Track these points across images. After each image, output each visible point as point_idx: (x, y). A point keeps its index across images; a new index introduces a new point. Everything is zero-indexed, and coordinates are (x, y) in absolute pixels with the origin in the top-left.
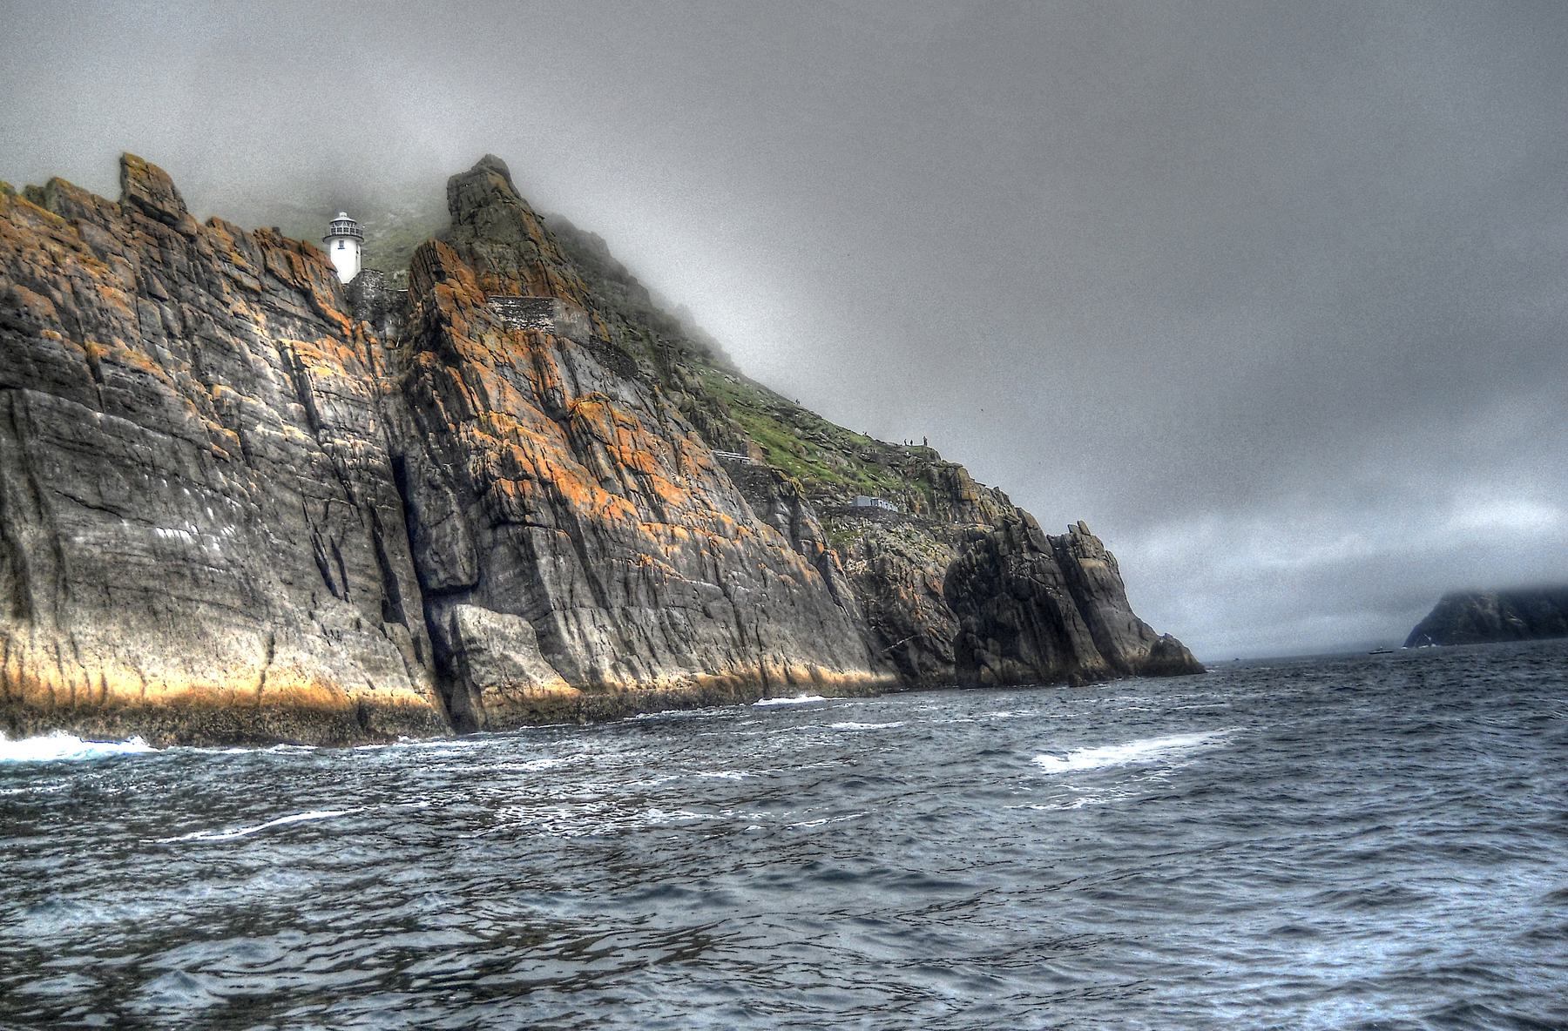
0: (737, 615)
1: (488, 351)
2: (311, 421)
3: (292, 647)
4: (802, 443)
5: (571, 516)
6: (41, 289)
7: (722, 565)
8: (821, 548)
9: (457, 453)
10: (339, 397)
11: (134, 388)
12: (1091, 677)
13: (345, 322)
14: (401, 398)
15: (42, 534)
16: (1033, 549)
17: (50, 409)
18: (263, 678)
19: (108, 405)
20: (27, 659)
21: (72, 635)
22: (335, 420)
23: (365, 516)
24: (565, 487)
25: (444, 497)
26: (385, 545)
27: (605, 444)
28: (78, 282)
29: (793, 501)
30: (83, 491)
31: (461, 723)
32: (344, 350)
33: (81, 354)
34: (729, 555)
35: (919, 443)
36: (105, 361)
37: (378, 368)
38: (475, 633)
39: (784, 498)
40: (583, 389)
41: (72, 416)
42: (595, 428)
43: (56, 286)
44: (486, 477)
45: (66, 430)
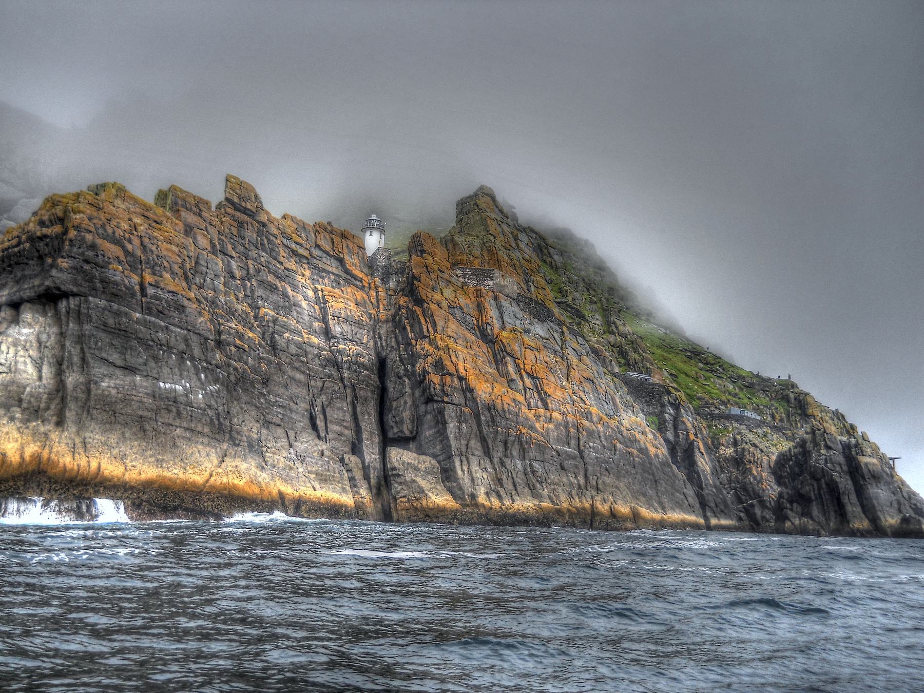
0: (586, 470)
1: (441, 296)
2: (327, 333)
3: (237, 460)
4: (703, 372)
5: (474, 400)
6: (118, 242)
7: (583, 439)
8: (692, 437)
9: (413, 357)
10: (346, 320)
11: (167, 301)
12: (855, 534)
13: (365, 278)
14: (390, 324)
15: (82, 380)
16: (828, 448)
17: (104, 309)
18: (211, 475)
19: (147, 309)
20: (55, 450)
21: (85, 438)
22: (342, 334)
23: (349, 391)
24: (473, 381)
25: (403, 384)
26: (358, 409)
27: (515, 358)
28: (146, 240)
29: (676, 406)
30: (115, 357)
31: (387, 516)
32: (360, 295)
33: (135, 279)
34: (590, 433)
35: (784, 377)
36: (151, 285)
37: (381, 306)
38: (396, 465)
39: (671, 404)
40: (507, 324)
41: (118, 314)
42: (508, 349)
43: (130, 241)
44: (424, 371)
45: (111, 321)
